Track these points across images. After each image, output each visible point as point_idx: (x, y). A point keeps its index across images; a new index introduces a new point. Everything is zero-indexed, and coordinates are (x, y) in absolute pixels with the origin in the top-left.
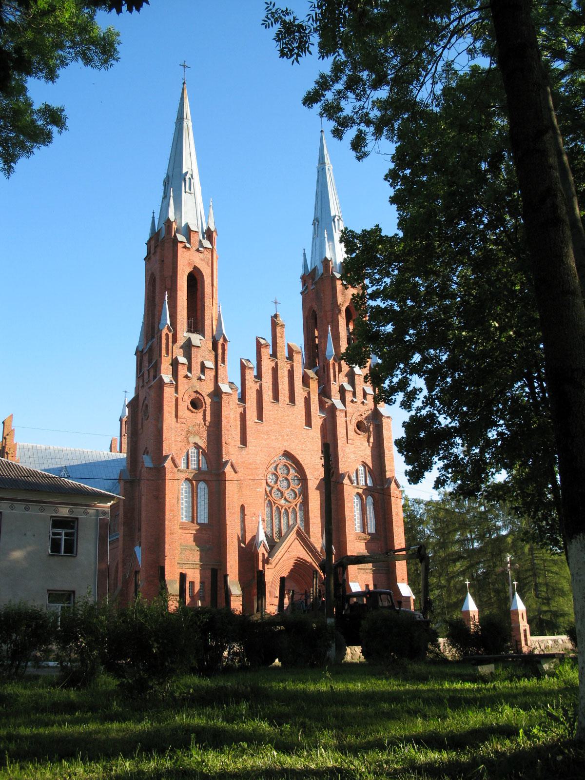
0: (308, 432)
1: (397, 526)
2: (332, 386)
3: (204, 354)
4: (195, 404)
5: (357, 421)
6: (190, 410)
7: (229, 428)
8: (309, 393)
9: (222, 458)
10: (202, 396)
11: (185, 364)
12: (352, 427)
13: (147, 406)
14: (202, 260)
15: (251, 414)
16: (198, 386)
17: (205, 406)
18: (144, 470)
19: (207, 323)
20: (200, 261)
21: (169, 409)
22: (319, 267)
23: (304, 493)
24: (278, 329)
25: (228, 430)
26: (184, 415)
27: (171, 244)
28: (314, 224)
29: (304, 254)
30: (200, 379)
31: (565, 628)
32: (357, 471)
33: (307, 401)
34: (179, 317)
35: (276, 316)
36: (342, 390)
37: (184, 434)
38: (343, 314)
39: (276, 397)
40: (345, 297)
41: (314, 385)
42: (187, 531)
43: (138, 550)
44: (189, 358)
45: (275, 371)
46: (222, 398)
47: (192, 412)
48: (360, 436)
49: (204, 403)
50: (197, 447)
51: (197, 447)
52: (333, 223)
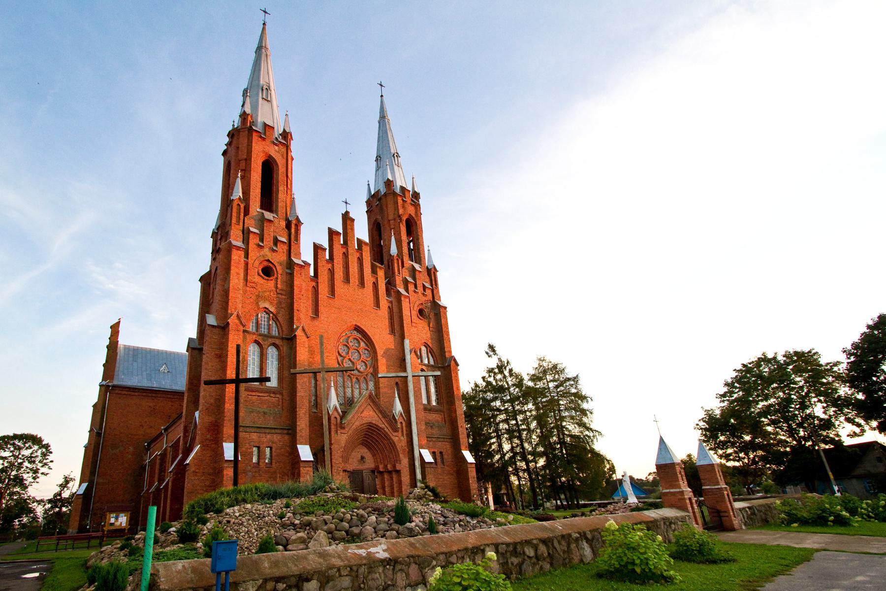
2: (397, 278)
3: (277, 229)
4: (267, 271)
6: (261, 276)
7: (301, 297)
10: (274, 265)
11: (285, 243)
12: (415, 313)
14: (276, 151)
15: (324, 289)
20: (275, 152)
21: (237, 270)
22: (382, 190)
23: (374, 365)
24: (349, 222)
26: (254, 280)
27: (247, 132)
28: (377, 160)
29: (369, 185)
32: (420, 349)
33: (375, 286)
35: (347, 213)
36: (406, 283)
39: (347, 279)
41: (381, 273)
42: (254, 394)
43: (197, 414)
45: (346, 255)
49: (275, 272)
50: (266, 310)
51: (266, 310)
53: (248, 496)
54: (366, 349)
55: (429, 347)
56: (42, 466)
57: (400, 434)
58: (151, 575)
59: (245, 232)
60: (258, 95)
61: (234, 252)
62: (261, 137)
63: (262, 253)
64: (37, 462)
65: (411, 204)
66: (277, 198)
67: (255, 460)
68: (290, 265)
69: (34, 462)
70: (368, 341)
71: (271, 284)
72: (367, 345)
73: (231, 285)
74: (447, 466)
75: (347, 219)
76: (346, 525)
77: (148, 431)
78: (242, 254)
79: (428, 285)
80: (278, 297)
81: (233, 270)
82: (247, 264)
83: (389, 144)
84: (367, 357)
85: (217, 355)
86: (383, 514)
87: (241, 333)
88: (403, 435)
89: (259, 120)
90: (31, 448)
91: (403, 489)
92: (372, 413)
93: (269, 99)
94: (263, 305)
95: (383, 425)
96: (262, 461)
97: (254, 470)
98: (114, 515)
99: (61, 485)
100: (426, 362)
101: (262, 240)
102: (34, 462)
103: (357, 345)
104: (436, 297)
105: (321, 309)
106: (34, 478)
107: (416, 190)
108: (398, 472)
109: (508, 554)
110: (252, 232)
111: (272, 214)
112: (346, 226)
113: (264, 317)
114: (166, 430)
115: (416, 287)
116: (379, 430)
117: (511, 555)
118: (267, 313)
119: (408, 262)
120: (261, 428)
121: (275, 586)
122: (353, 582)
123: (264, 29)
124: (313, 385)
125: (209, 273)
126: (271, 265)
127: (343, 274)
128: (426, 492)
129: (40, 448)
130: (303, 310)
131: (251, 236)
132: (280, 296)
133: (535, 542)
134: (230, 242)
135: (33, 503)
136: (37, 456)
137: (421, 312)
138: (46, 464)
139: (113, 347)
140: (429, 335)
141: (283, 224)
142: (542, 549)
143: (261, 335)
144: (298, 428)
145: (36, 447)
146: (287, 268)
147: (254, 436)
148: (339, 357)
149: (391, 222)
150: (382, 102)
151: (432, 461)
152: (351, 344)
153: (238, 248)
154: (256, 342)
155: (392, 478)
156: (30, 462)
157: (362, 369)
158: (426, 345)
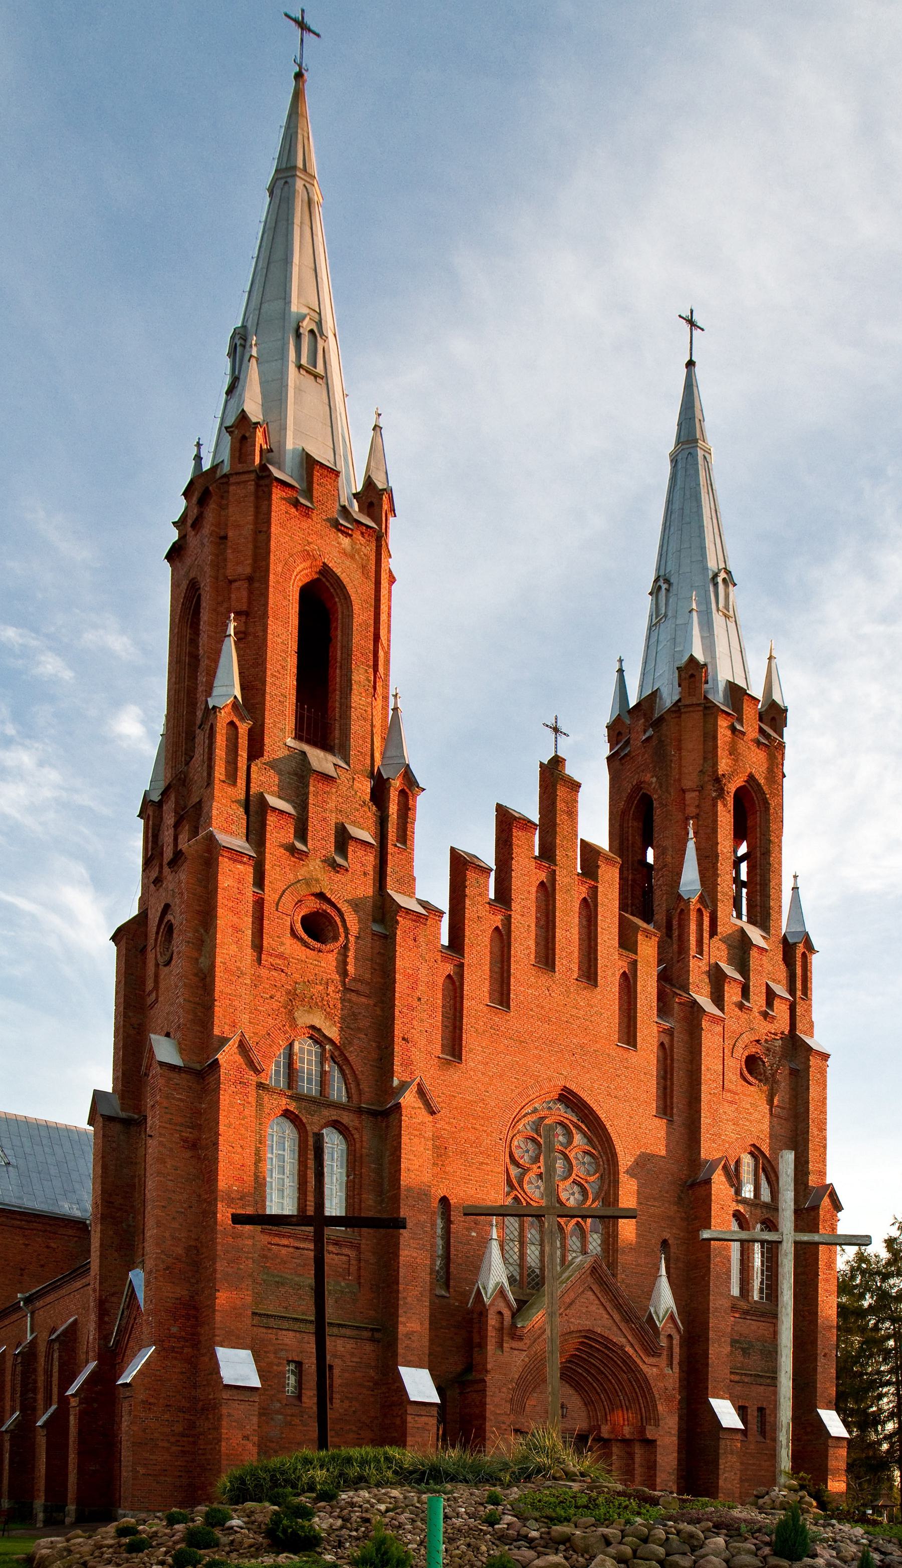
1: (827, 1291)
2: (693, 963)
5: (746, 1054)
6: (301, 940)
7: (415, 1003)
8: (634, 964)
9: (390, 1073)
10: (338, 910)
12: (735, 1064)
13: (170, 928)
17: (346, 937)
18: (156, 1070)
19: (357, 728)
24: (561, 792)
26: (281, 949)
27: (251, 487)
28: (655, 591)
29: (621, 671)
30: (335, 866)
31: (857, 1543)
33: (628, 984)
34: (271, 668)
35: (557, 762)
37: (280, 996)
38: (730, 800)
42: (285, 1242)
43: (137, 1277)
44: (743, 968)
45: (547, 891)
46: (397, 922)
47: (307, 945)
48: (752, 1088)
49: (341, 930)
50: (317, 1036)
51: (317, 1036)
52: (711, 589)
53: (371, 1471)
54: (586, 1153)
57: (663, 1361)
59: (252, 808)
61: (225, 865)
65: (758, 743)
66: (346, 707)
70: (598, 1136)
72: (590, 1141)
73: (219, 960)
78: (247, 871)
79: (780, 990)
80: (350, 1001)
81: (224, 918)
82: (259, 904)
85: (185, 1140)
86: (740, 1535)
87: (252, 1091)
88: (671, 1365)
89: (289, 446)
92: (595, 1308)
93: (320, 369)
94: (305, 1018)
97: (289, 1412)
100: (748, 1192)
104: (799, 1025)
105: (470, 1039)
107: (776, 697)
108: (650, 1444)
110: (274, 809)
111: (330, 757)
112: (554, 804)
113: (310, 1052)
114: (28, 1300)
115: (745, 992)
118: (316, 1042)
125: (140, 921)
132: (354, 997)
134: (211, 837)
141: (365, 787)
149: (689, 796)
153: (236, 855)
155: (631, 1455)
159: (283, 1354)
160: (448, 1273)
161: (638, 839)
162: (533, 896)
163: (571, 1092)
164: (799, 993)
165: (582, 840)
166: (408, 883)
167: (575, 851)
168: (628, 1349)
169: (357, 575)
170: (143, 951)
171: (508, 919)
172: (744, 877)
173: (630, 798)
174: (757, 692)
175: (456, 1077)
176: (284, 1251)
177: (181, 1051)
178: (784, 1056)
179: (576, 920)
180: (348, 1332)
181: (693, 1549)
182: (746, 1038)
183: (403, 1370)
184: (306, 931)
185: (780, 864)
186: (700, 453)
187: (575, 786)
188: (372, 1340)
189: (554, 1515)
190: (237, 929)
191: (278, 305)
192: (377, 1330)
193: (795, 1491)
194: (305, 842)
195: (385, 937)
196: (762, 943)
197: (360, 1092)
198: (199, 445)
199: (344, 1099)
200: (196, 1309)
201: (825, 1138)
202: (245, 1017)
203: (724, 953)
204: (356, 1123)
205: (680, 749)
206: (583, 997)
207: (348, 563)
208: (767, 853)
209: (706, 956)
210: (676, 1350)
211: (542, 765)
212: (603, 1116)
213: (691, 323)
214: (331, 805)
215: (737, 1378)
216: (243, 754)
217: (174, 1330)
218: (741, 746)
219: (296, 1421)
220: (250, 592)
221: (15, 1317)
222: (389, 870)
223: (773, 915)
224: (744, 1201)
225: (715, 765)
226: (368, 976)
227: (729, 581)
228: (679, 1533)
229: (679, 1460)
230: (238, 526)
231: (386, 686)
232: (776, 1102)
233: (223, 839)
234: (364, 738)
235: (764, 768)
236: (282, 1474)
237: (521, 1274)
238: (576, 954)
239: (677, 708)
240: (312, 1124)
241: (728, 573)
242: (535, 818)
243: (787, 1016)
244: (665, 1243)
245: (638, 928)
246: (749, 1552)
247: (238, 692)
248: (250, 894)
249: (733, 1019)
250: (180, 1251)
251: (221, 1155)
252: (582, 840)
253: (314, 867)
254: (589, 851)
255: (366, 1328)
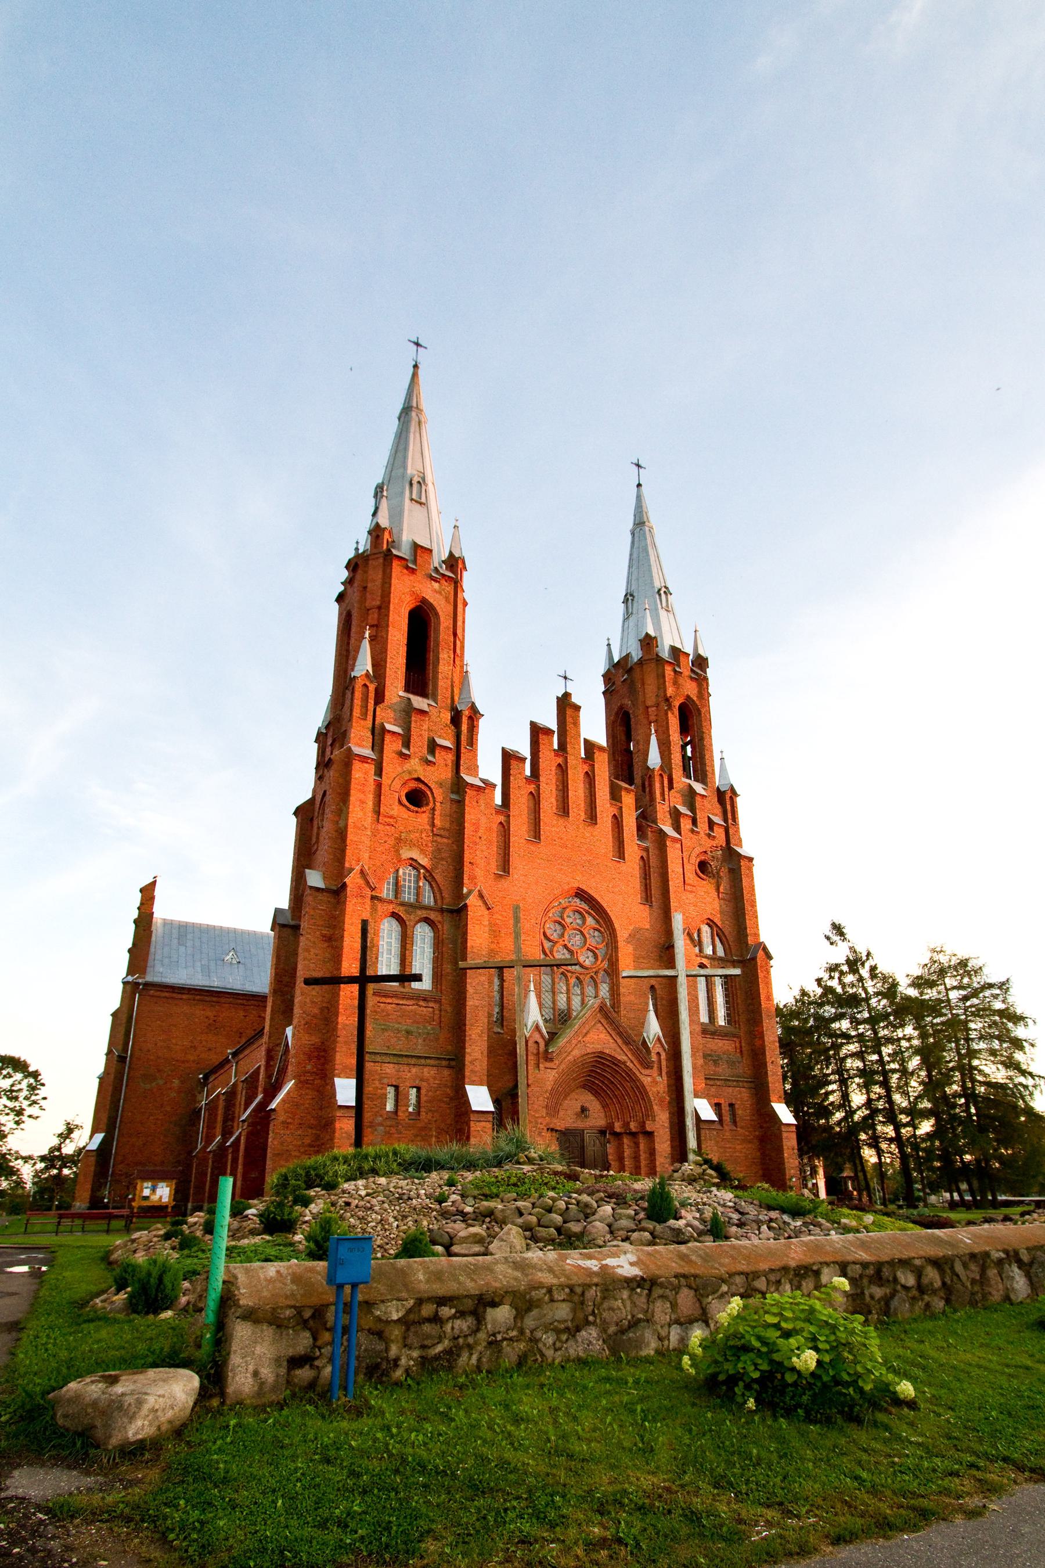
0: (618, 865)
2: (659, 807)
4: (416, 798)
7: (478, 840)
10: (429, 787)
11: (450, 749)
12: (691, 868)
14: (435, 591)
16: (421, 771)
17: (434, 801)
20: (434, 593)
22: (634, 654)
23: (611, 956)
24: (569, 712)
25: (475, 843)
27: (381, 560)
28: (626, 601)
29: (609, 645)
33: (618, 822)
35: (567, 695)
37: (391, 842)
38: (676, 712)
39: (564, 810)
40: (678, 688)
41: (628, 800)
42: (389, 1000)
44: (692, 808)
45: (563, 770)
47: (409, 809)
50: (414, 864)
51: (414, 864)
53: (381, 1165)
54: (595, 929)
55: (717, 926)
56: (30, 1105)
58: (224, 1282)
59: (377, 732)
60: (402, 493)
61: (357, 765)
62: (407, 568)
63: (407, 766)
64: (21, 1099)
65: (692, 678)
66: (436, 672)
67: (390, 1107)
68: (459, 786)
69: (16, 1098)
71: (422, 819)
72: (598, 922)
73: (350, 821)
74: (742, 1128)
75: (566, 706)
76: (558, 1219)
77: (203, 1056)
78: (371, 768)
79: (717, 820)
81: (354, 796)
82: (379, 786)
83: (650, 571)
84: (598, 943)
85: (324, 936)
86: (625, 1203)
87: (368, 901)
88: (661, 1075)
90: (11, 1077)
91: (657, 1163)
92: (604, 1036)
93: (423, 500)
94: (406, 853)
95: (624, 1055)
96: (402, 1109)
98: (150, 1184)
99: (60, 1135)
100: (709, 951)
101: (407, 744)
102: (16, 1098)
103: (579, 921)
104: (732, 841)
106: (17, 1123)
107: (701, 652)
108: (650, 1135)
109: (865, 1281)
110: (389, 731)
111: (426, 701)
112: (565, 718)
113: (410, 875)
114: (235, 1054)
115: (694, 822)
116: (616, 1065)
117: (870, 1282)
118: (414, 868)
119: (681, 781)
120: (402, 1056)
121: (437, 1312)
122: (574, 1310)
123: (415, 375)
124: (496, 988)
125: (311, 802)
126: (423, 787)
127: (557, 801)
128: (704, 1170)
129: (26, 1077)
130: (482, 863)
131: (388, 738)
132: (439, 839)
133: (917, 1262)
134: (350, 749)
135: (17, 1159)
136: (20, 1090)
137: (703, 866)
138: (35, 1102)
139: (144, 922)
140: (716, 905)
141: (447, 716)
142: (932, 1275)
143: (402, 904)
144: (468, 1059)
145: (19, 1076)
146: (452, 792)
147: (389, 1069)
148: (545, 942)
150: (639, 498)
151: (714, 1118)
152: (568, 920)
153: (364, 759)
154: (394, 915)
155: (637, 1145)
156: (10, 1099)
157: (587, 963)
158: (711, 923)
159: (385, 1081)
160: (502, 1016)
161: (624, 738)
162: (553, 773)
163: (583, 891)
164: (730, 821)
165: (585, 740)
166: (474, 769)
167: (579, 745)
168: (629, 1064)
169: (443, 602)
170: (312, 820)
171: (538, 787)
172: (689, 754)
173: (617, 714)
174: (689, 649)
175: (506, 885)
176: (389, 1007)
177: (325, 878)
178: (724, 860)
179: (582, 785)
180: (432, 1062)
181: (587, 1216)
182: (698, 850)
183: (468, 1087)
184: (411, 803)
185: (711, 745)
186: (647, 529)
187: (577, 708)
188: (449, 1067)
189: (488, 1192)
190: (362, 802)
191: (401, 470)
192: (452, 1059)
193: (701, 1165)
194: (408, 748)
195: (459, 802)
196: (703, 792)
197: (442, 898)
198: (357, 543)
199: (432, 904)
200: (325, 1051)
201: (756, 912)
202: (366, 855)
203: (680, 800)
204: (439, 918)
205: (643, 684)
206: (587, 832)
207: (437, 596)
208: (702, 739)
209: (667, 802)
210: (664, 1063)
211: (558, 698)
212: (605, 905)
213: (638, 466)
214: (425, 727)
215: (711, 1082)
216: (371, 702)
217: (309, 1067)
218: (681, 681)
219: (393, 1130)
220: (379, 615)
221: (227, 1067)
222: (462, 762)
223: (709, 775)
224: (706, 957)
225: (665, 691)
226: (447, 825)
227: (667, 593)
228: (578, 1203)
229: (672, 1147)
230: (374, 581)
231: (462, 660)
232: (721, 890)
233: (356, 750)
234: (446, 689)
235: (696, 691)
236: (314, 1170)
237: (554, 1015)
238: (583, 805)
239: (641, 662)
240: (410, 920)
241: (666, 587)
242: (554, 727)
243: (723, 836)
244: (652, 987)
245: (621, 788)
246: (629, 1217)
247: (370, 668)
248: (372, 781)
249: (688, 840)
250: (316, 1011)
251: (345, 944)
252: (585, 740)
253: (415, 765)
254: (590, 746)
255: (444, 1059)
